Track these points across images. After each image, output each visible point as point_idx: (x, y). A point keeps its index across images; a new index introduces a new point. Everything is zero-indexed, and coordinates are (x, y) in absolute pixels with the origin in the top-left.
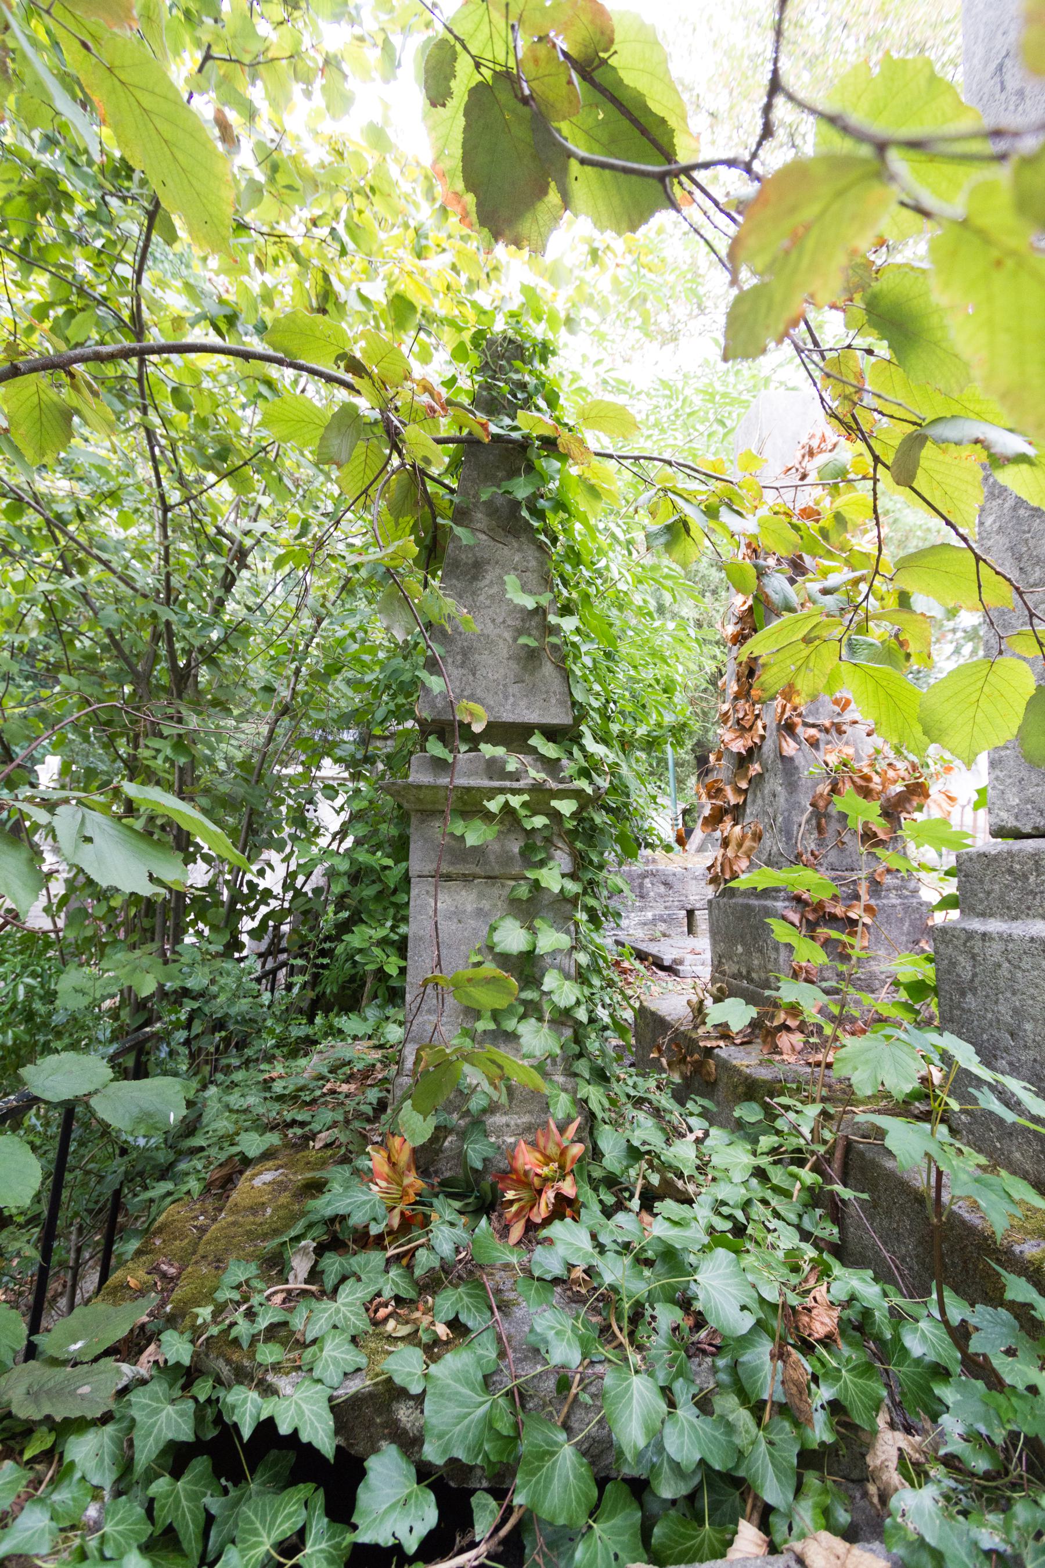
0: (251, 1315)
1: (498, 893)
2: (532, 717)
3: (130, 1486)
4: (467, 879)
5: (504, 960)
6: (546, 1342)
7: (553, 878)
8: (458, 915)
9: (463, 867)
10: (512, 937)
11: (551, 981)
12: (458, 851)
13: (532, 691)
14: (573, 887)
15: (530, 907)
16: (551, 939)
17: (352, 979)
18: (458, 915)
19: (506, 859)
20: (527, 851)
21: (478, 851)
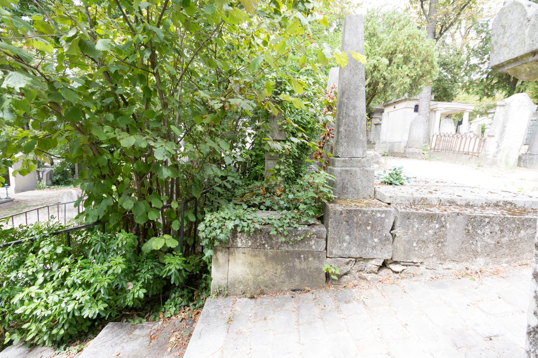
0: (279, 170)
1: (276, 161)
2: (281, 139)
3: (10, 208)
4: (272, 160)
5: (276, 169)
6: (495, 68)
7: (282, 160)
8: (271, 164)
9: (271, 158)
10: (277, 167)
11: (281, 172)
12: (271, 156)
13: (281, 136)
14: (285, 161)
15: (280, 163)
16: (282, 167)
17: (256, 176)
18: (271, 164)
19: (277, 157)
20: (280, 156)
21: (273, 156)
